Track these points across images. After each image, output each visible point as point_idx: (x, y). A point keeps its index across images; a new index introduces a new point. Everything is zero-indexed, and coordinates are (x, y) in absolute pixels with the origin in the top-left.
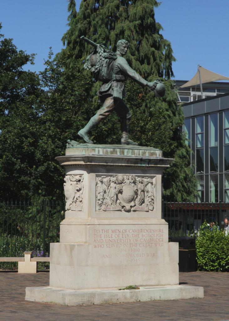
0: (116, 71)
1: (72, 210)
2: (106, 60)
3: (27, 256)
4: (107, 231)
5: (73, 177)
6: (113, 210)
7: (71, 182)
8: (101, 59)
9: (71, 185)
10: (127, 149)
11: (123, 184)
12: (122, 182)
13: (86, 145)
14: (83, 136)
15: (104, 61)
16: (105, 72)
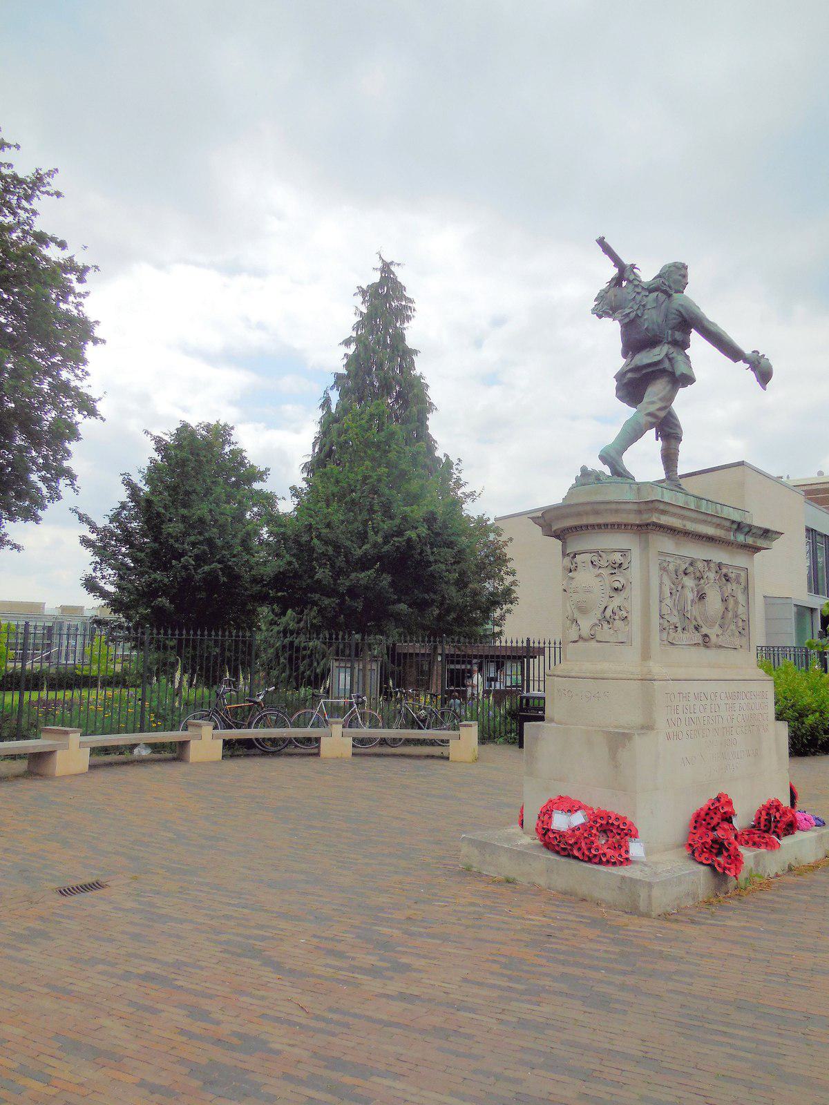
0: (674, 321)
1: (597, 641)
2: (655, 294)
3: (337, 729)
6: (687, 643)
8: (638, 293)
9: (598, 576)
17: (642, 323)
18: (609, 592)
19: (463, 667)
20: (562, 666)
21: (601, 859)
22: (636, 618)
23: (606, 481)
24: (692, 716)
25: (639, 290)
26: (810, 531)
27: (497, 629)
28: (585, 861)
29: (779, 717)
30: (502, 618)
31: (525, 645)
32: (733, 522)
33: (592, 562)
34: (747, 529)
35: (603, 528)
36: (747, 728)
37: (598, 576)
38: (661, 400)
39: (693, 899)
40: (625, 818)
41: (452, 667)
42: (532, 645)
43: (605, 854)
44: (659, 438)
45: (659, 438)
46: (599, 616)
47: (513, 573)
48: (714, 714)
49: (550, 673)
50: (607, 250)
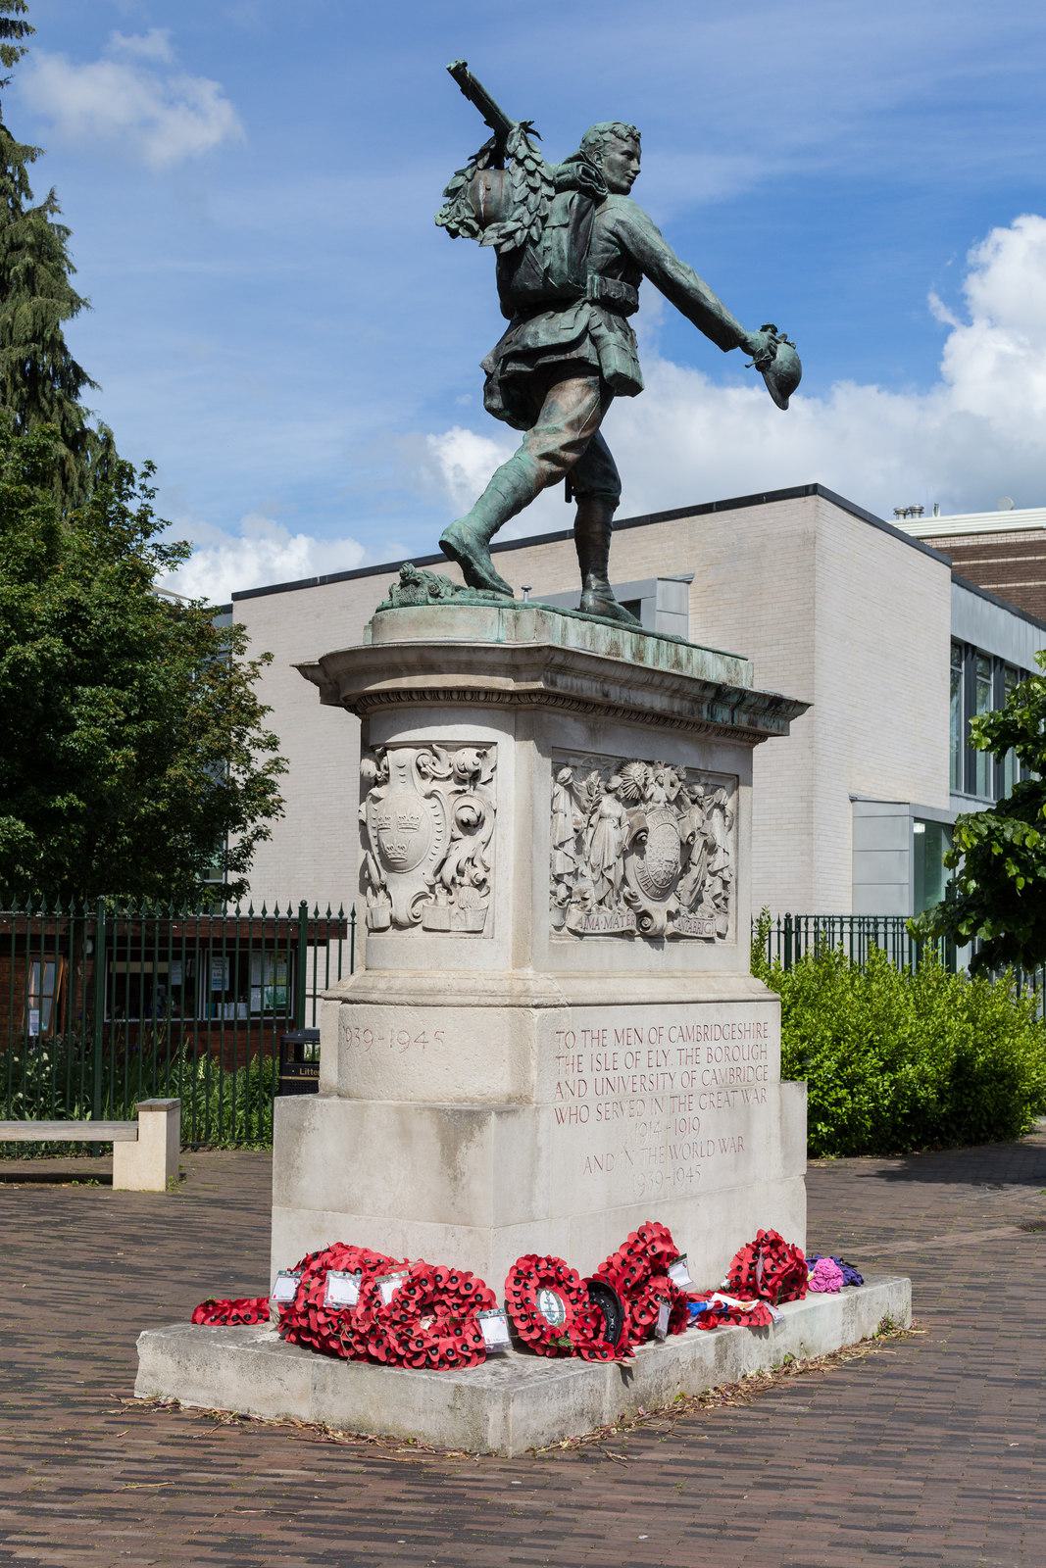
1: (426, 929)
2: (568, 195)
4: (599, 1038)
5: (436, 755)
7: (429, 786)
8: (535, 190)
9: (428, 796)
10: (653, 635)
11: (642, 807)
12: (642, 797)
13: (493, 598)
14: (471, 552)
15: (550, 198)
16: (560, 251)
17: (538, 255)
18: (451, 828)
19: (148, 967)
20: (350, 981)
21: (428, 1357)
22: (504, 882)
23: (453, 599)
24: (611, 1075)
25: (536, 182)
26: (962, 649)
27: (233, 877)
28: (391, 1365)
29: (788, 1074)
30: (247, 849)
31: (296, 914)
32: (706, 685)
33: (419, 768)
34: (735, 699)
35: (442, 697)
36: (722, 1096)
37: (428, 796)
38: (571, 425)
39: (592, 1421)
40: (470, 1274)
41: (120, 967)
42: (311, 915)
43: (435, 1347)
44: (573, 497)
45: (573, 497)
46: (430, 878)
47: (272, 743)
48: (655, 1070)
49: (329, 994)
50: (472, 90)
